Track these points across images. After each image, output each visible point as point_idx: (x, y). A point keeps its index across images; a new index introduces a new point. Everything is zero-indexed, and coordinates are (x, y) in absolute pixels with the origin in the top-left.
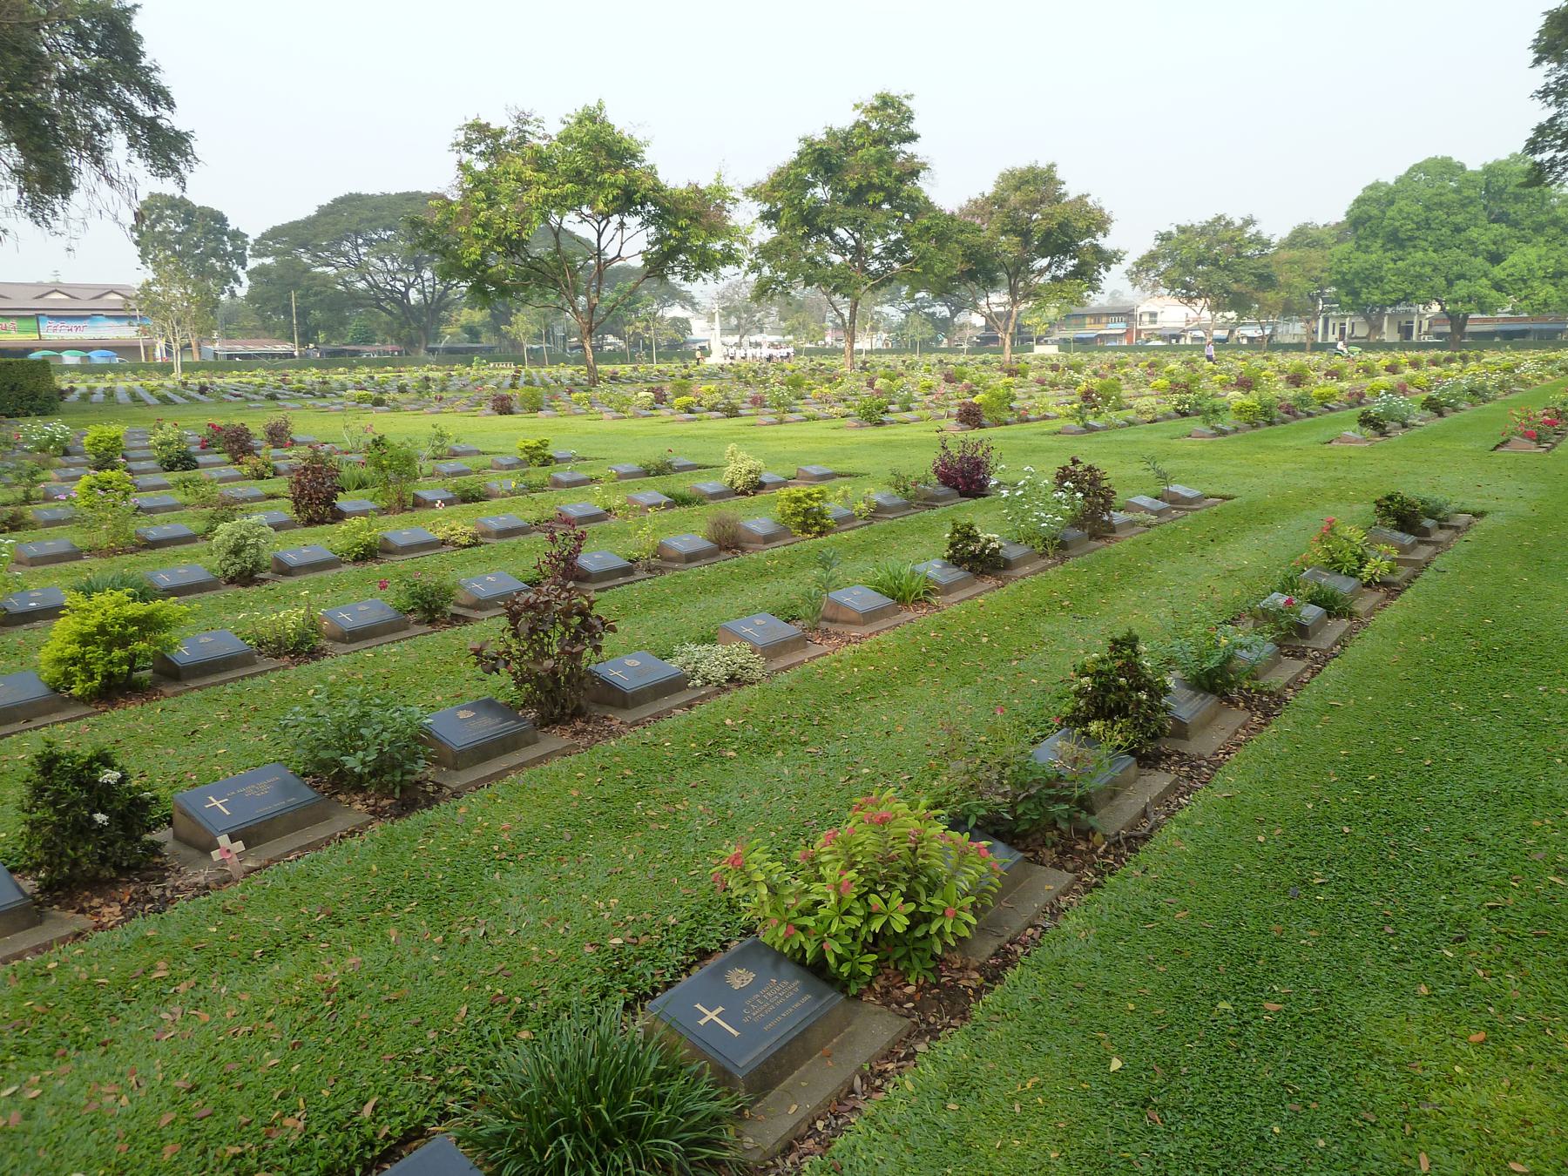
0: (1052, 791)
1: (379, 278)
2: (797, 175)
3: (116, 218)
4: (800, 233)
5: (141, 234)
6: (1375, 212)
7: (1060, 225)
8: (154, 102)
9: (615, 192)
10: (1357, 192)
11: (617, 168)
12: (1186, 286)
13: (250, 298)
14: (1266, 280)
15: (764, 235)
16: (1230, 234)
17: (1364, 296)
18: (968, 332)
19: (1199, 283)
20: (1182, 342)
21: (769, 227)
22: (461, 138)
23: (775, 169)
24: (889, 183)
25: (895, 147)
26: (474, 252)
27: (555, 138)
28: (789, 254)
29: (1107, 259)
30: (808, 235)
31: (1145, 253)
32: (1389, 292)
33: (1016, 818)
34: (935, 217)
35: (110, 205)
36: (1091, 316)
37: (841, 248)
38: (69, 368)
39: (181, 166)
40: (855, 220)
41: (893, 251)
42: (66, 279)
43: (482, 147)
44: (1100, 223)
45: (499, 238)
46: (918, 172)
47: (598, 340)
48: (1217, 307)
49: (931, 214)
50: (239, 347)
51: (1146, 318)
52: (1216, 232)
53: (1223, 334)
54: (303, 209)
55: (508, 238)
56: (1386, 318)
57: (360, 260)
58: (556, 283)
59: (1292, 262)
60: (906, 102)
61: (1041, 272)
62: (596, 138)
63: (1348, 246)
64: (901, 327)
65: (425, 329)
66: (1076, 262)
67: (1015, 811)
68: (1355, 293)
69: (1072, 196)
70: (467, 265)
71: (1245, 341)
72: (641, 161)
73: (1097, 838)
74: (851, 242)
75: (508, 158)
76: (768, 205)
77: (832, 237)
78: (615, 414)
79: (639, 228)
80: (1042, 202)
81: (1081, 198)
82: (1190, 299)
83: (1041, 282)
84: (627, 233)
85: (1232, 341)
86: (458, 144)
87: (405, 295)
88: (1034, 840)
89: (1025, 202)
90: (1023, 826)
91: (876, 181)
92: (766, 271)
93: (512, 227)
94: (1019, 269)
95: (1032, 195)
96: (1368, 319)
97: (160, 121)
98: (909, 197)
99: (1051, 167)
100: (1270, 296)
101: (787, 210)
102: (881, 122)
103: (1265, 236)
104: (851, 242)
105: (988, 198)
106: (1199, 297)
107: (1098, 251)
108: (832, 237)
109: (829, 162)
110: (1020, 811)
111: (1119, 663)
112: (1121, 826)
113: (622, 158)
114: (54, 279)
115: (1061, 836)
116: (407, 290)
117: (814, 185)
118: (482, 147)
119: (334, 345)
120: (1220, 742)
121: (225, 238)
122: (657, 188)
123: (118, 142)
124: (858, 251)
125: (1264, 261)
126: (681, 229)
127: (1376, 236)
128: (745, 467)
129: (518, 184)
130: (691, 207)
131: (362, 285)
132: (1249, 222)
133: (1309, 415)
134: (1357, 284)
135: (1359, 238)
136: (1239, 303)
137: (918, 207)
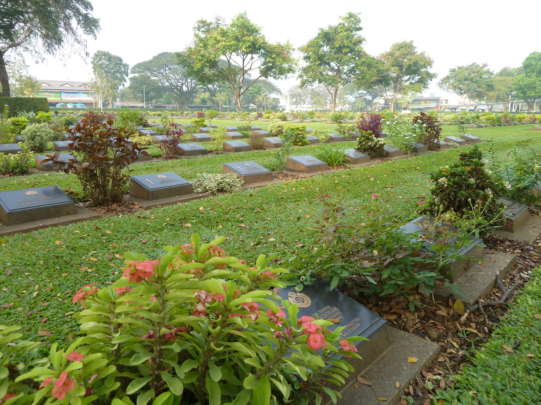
0: (417, 259)
1: (173, 81)
2: (317, 42)
3: (80, 54)
4: (317, 63)
5: (94, 64)
6: (534, 62)
7: (414, 63)
8: (86, 8)
9: (249, 44)
10: (527, 55)
11: (250, 35)
12: (460, 89)
13: (130, 87)
14: (490, 87)
15: (304, 64)
16: (478, 69)
17: (528, 94)
18: (378, 106)
19: (465, 87)
20: (457, 110)
21: (307, 62)
22: (196, 26)
23: (309, 40)
24: (351, 45)
25: (354, 33)
26: (198, 66)
27: (229, 25)
28: (313, 71)
29: (431, 76)
30: (320, 65)
31: (445, 76)
32: (538, 93)
33: (381, 282)
34: (367, 58)
35: (78, 50)
36: (423, 100)
37: (332, 69)
38: (69, 109)
39: (95, 31)
40: (338, 59)
41: (352, 71)
42: (72, 80)
43: (204, 29)
44: (429, 63)
45: (207, 61)
46: (362, 41)
47: (247, 105)
48: (472, 97)
49: (366, 57)
50: (126, 104)
51: (444, 102)
52: (472, 69)
53: (473, 108)
54: (148, 57)
55: (210, 60)
56: (535, 104)
57: (166, 75)
58: (228, 80)
59: (501, 81)
60: (358, 16)
61: (406, 81)
62: (243, 24)
63: (523, 75)
64: (354, 103)
65: (188, 99)
66: (419, 77)
67: (381, 275)
68: (524, 93)
69: (419, 53)
70: (196, 70)
71: (481, 111)
72: (260, 34)
73: (458, 306)
74: (336, 68)
75: (212, 32)
76: (306, 54)
77: (329, 66)
78: (240, 119)
79: (258, 58)
80: (407, 55)
81: (422, 53)
82: (461, 94)
83: (406, 84)
84: (254, 60)
85: (476, 110)
86: (195, 28)
87: (182, 87)
88: (398, 303)
89: (401, 55)
90: (387, 291)
91: (346, 44)
92: (305, 78)
93: (212, 56)
94: (397, 80)
95: (404, 52)
96: (528, 103)
97: (88, 15)
98: (358, 51)
99: (412, 42)
100: (492, 93)
101: (313, 55)
102: (349, 24)
103: (491, 71)
104: (336, 68)
105: (387, 53)
106: (465, 93)
107: (428, 74)
108: (329, 66)
109: (329, 37)
110: (385, 275)
111: (468, 169)
112: (478, 294)
113: (253, 32)
114: (68, 81)
115: (423, 300)
116: (182, 85)
117: (323, 46)
118: (204, 29)
119: (158, 104)
120: (537, 235)
121: (122, 66)
122: (264, 43)
123: (74, 22)
124: (339, 71)
125: (490, 80)
126: (273, 58)
127: (533, 71)
128: (277, 125)
129: (215, 41)
130: (277, 50)
131: (167, 84)
132: (485, 65)
133: (515, 124)
134: (526, 89)
135: (527, 73)
136: (480, 96)
137: (360, 54)
